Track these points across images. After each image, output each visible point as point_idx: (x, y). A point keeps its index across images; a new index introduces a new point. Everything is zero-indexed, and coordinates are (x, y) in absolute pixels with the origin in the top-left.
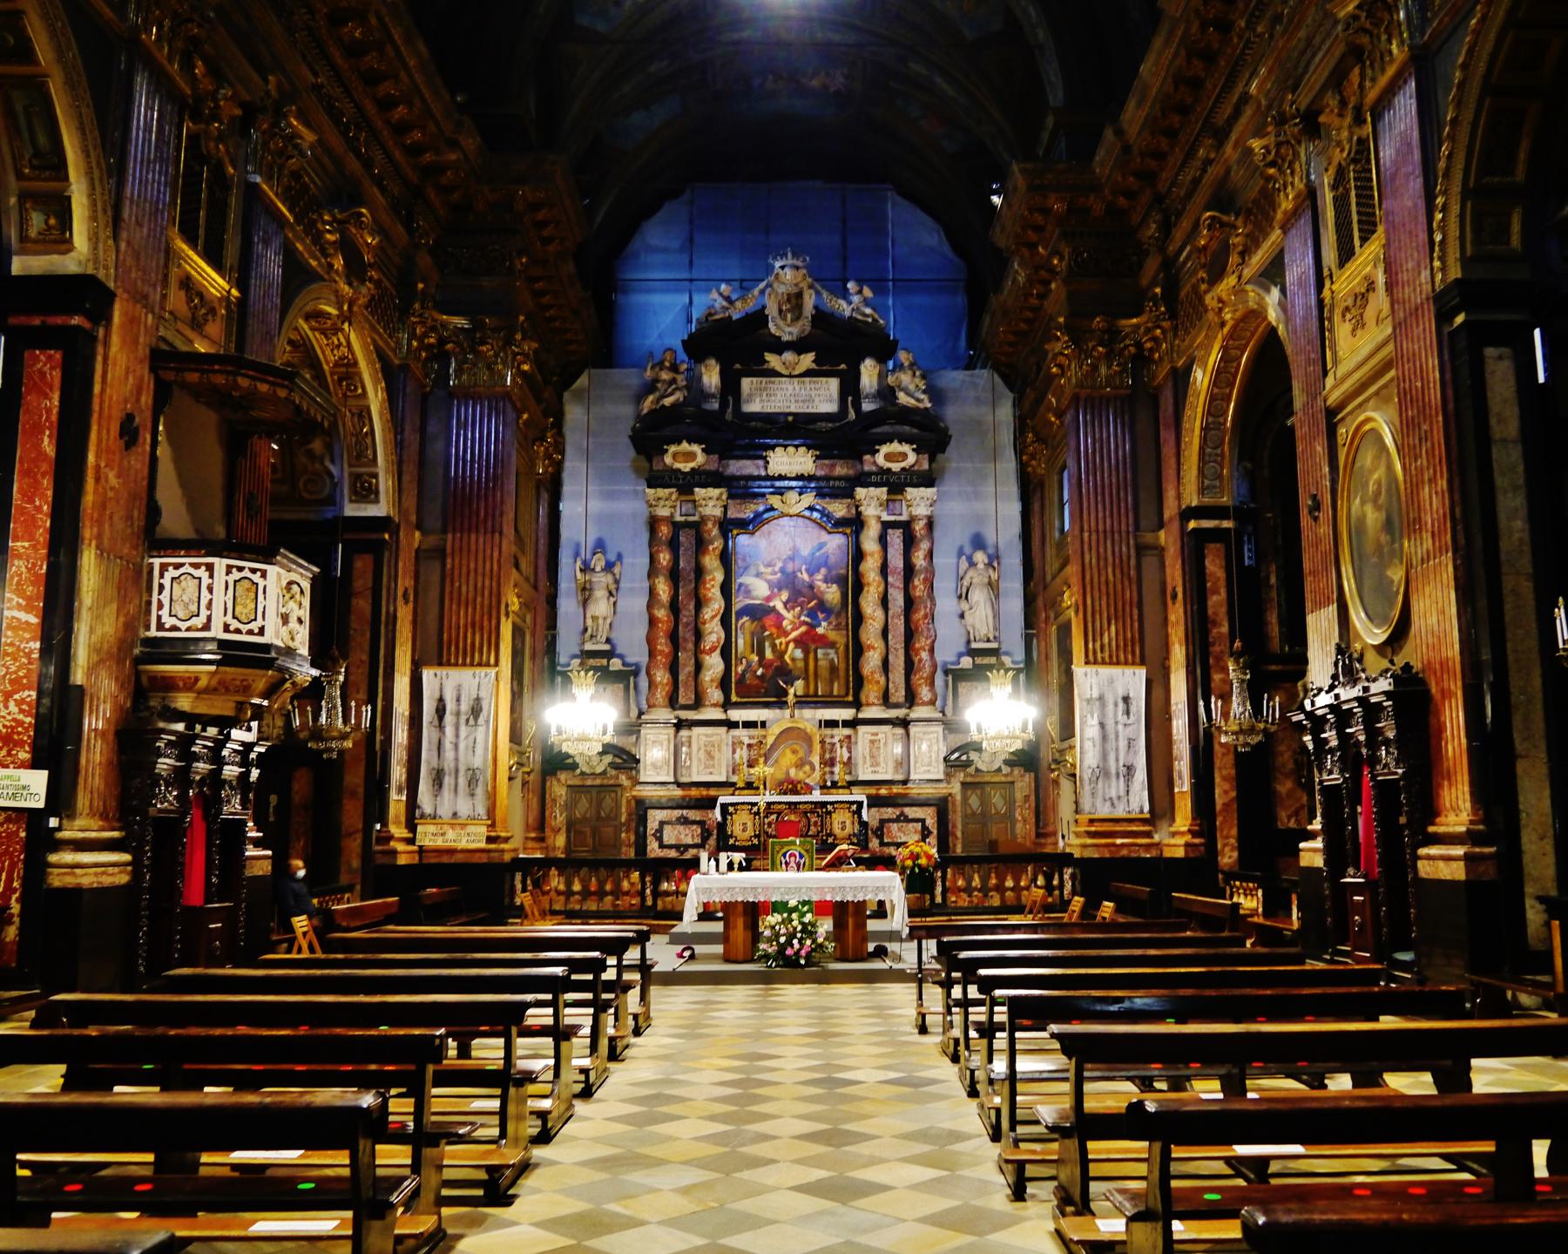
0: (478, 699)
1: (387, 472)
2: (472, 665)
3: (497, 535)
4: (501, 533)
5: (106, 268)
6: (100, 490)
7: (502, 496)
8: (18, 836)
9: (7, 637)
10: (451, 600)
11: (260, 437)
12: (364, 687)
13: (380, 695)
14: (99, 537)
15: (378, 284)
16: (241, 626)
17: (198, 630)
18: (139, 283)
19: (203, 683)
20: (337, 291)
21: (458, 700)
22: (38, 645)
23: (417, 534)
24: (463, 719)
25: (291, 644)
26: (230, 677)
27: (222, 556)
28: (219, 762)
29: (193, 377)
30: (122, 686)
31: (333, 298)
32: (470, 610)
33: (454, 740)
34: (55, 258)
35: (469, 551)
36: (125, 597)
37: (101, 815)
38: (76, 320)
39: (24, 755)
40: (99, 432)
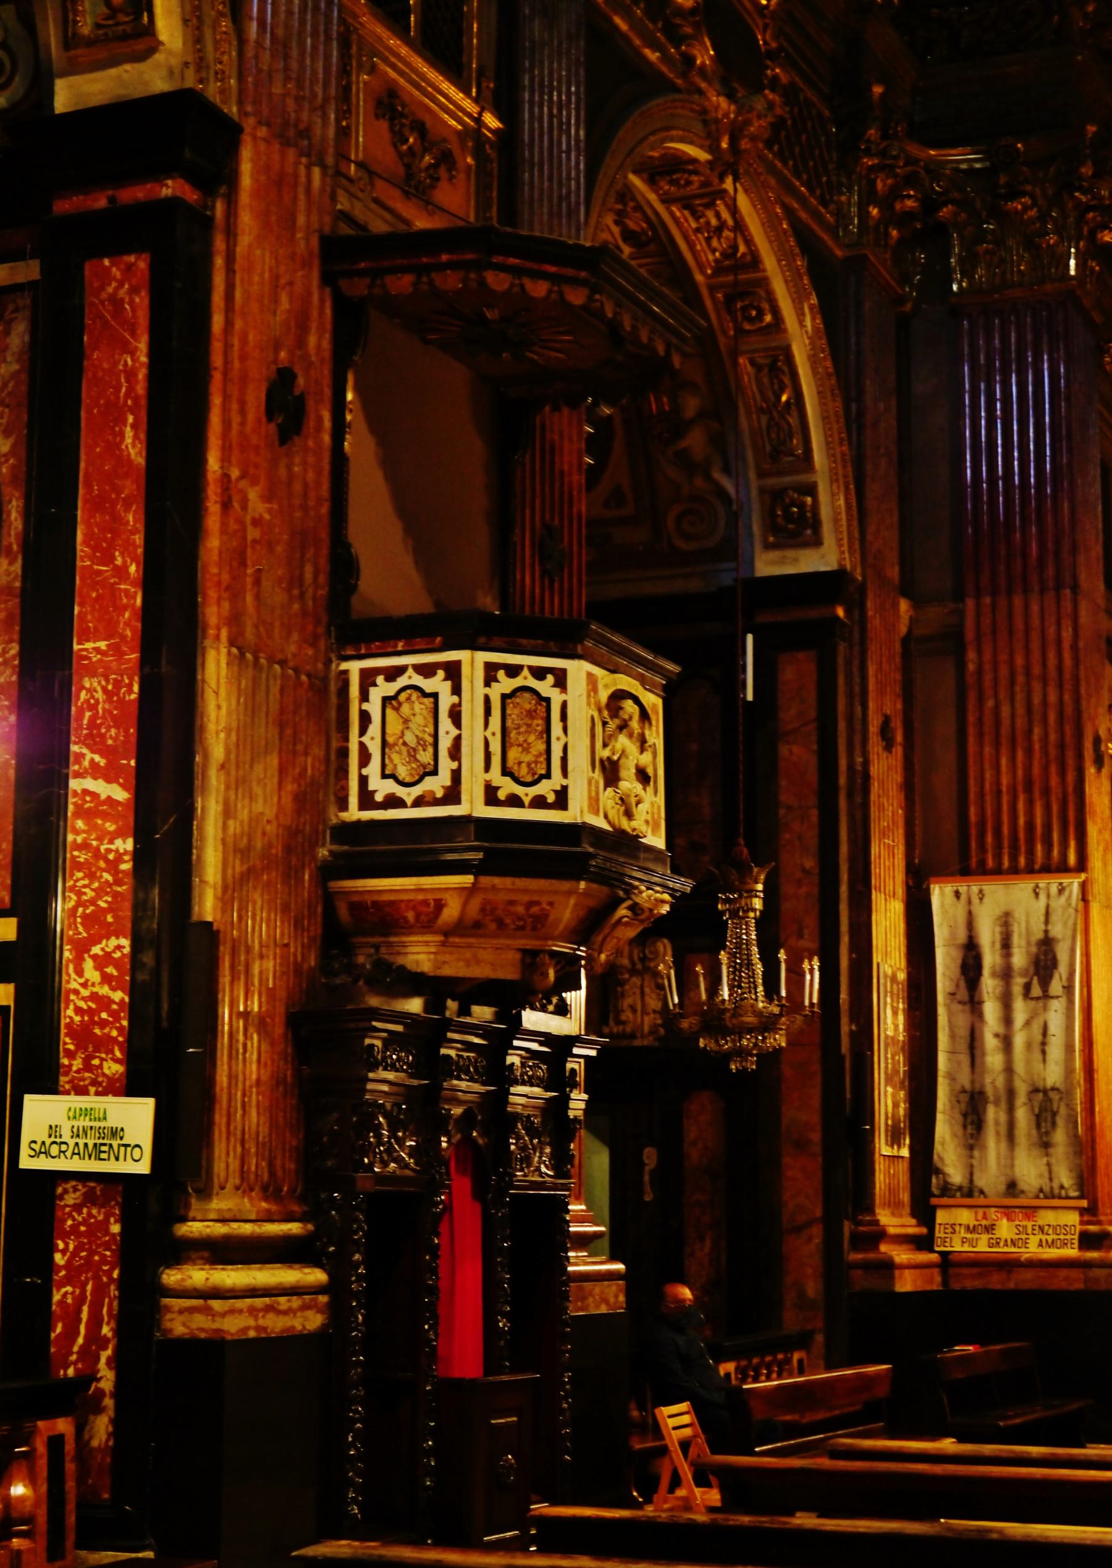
0: (1047, 943)
1: (834, 479)
2: (1031, 870)
3: (1068, 592)
4: (1075, 588)
5: (221, 76)
6: (233, 526)
7: (1073, 512)
8: (107, 1231)
9: (77, 832)
10: (980, 735)
11: (556, 408)
12: (811, 923)
13: (845, 940)
14: (234, 620)
15: (789, 93)
16: (519, 790)
17: (437, 802)
18: (291, 103)
19: (451, 912)
20: (704, 112)
21: (1006, 945)
22: (129, 845)
23: (904, 605)
24: (1018, 982)
25: (625, 824)
26: (503, 897)
27: (475, 647)
28: (502, 1077)
29: (402, 284)
30: (297, 924)
31: (698, 127)
32: (1020, 755)
33: (1001, 1030)
34: (127, 70)
35: (1011, 632)
36: (295, 740)
37: (265, 1188)
38: (169, 189)
39: (113, 1068)
40: (225, 409)
